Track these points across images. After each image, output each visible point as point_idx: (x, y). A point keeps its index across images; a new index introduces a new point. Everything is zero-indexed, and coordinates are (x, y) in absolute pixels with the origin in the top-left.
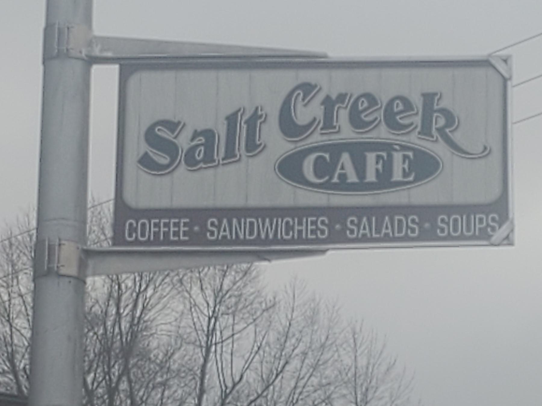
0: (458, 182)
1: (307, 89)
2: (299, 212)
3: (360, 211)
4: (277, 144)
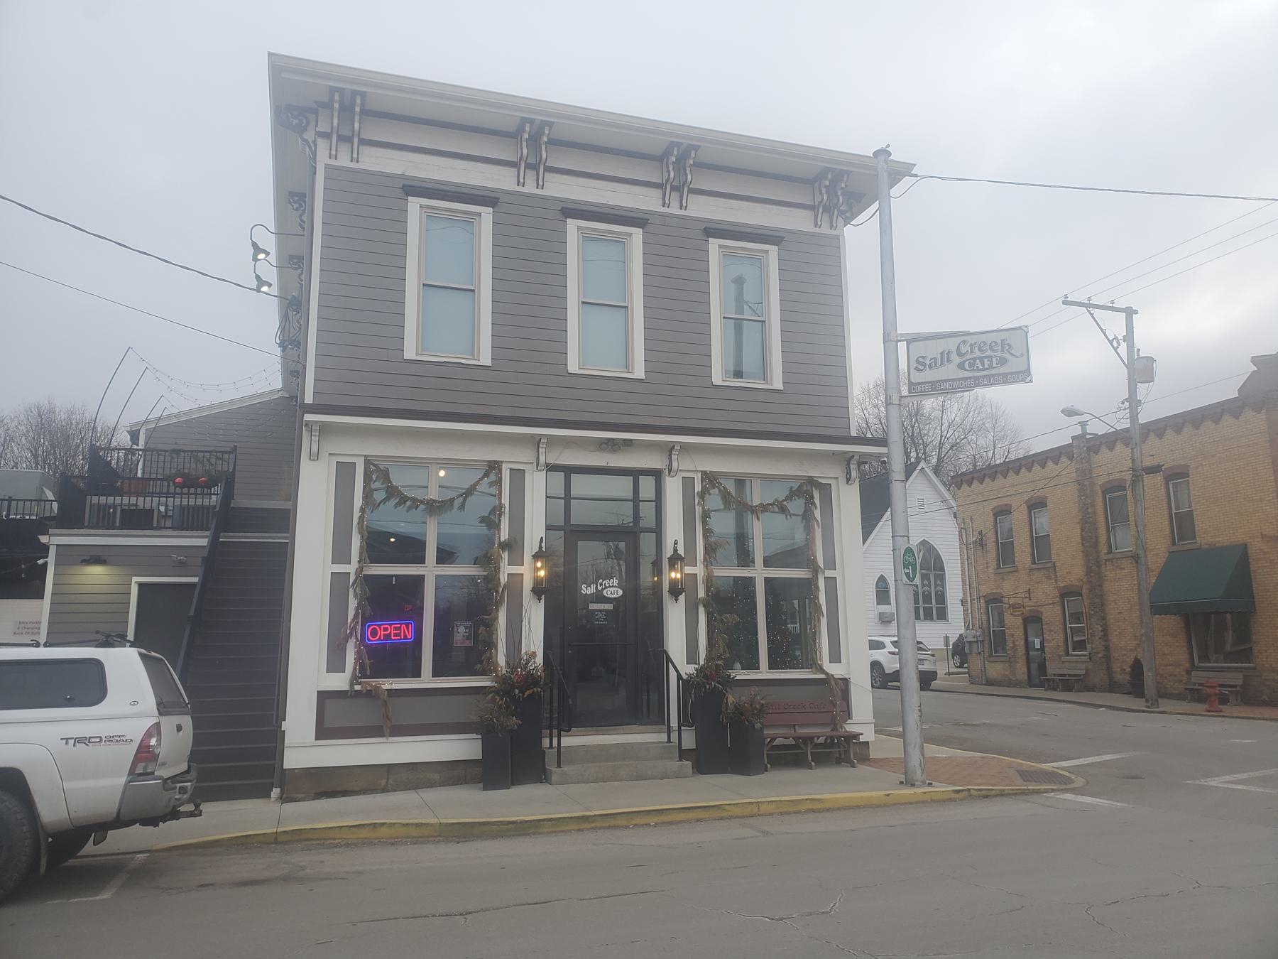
0: (1014, 365)
1: (964, 342)
2: (965, 379)
3: (983, 377)
4: (956, 360)
